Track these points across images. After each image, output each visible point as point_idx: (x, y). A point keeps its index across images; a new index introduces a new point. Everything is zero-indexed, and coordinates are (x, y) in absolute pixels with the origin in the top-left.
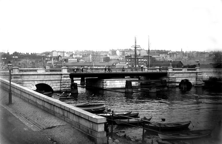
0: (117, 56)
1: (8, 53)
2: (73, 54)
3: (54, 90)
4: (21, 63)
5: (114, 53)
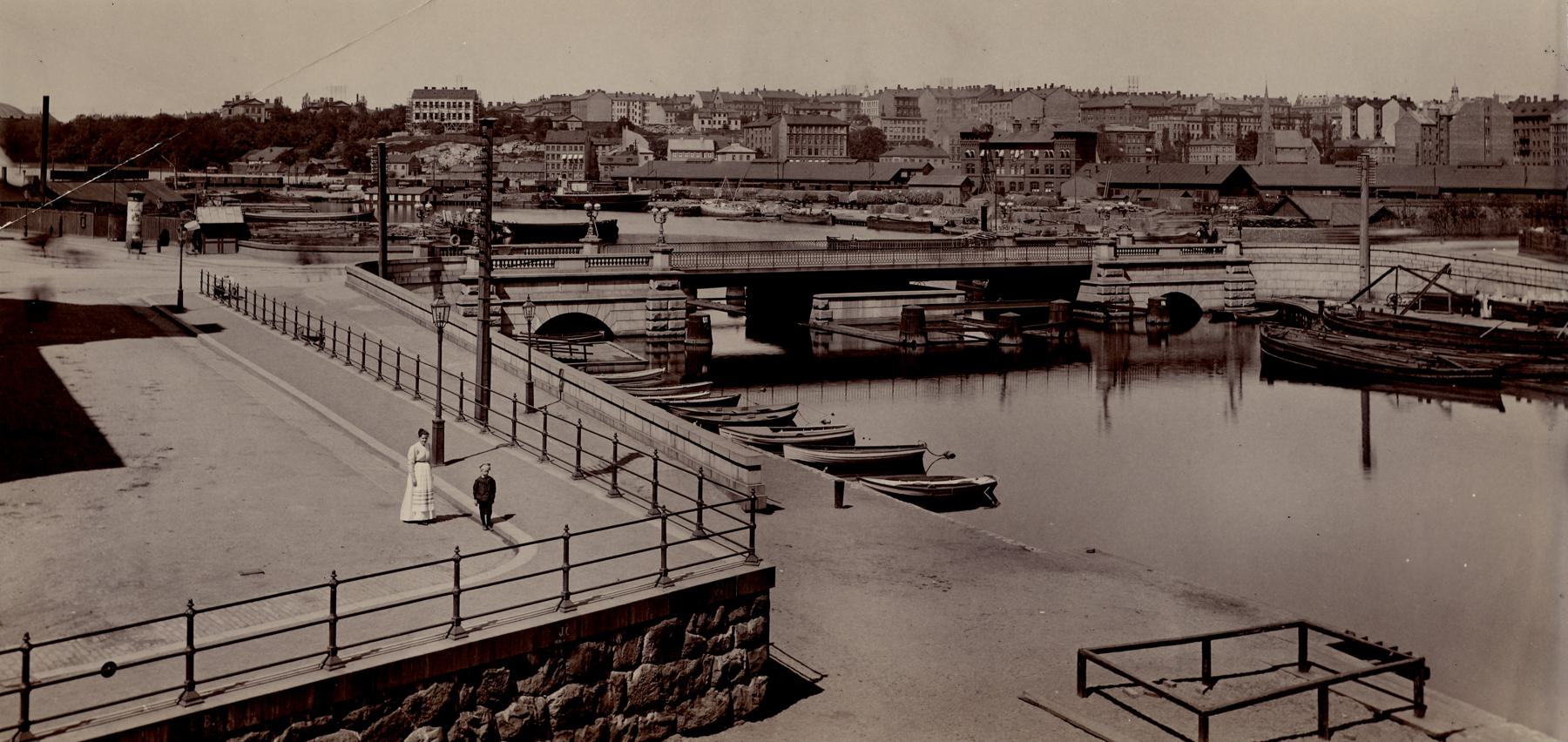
0: (921, 125)
1: (361, 106)
2: (694, 110)
3: (614, 329)
4: (427, 160)
5: (905, 104)
